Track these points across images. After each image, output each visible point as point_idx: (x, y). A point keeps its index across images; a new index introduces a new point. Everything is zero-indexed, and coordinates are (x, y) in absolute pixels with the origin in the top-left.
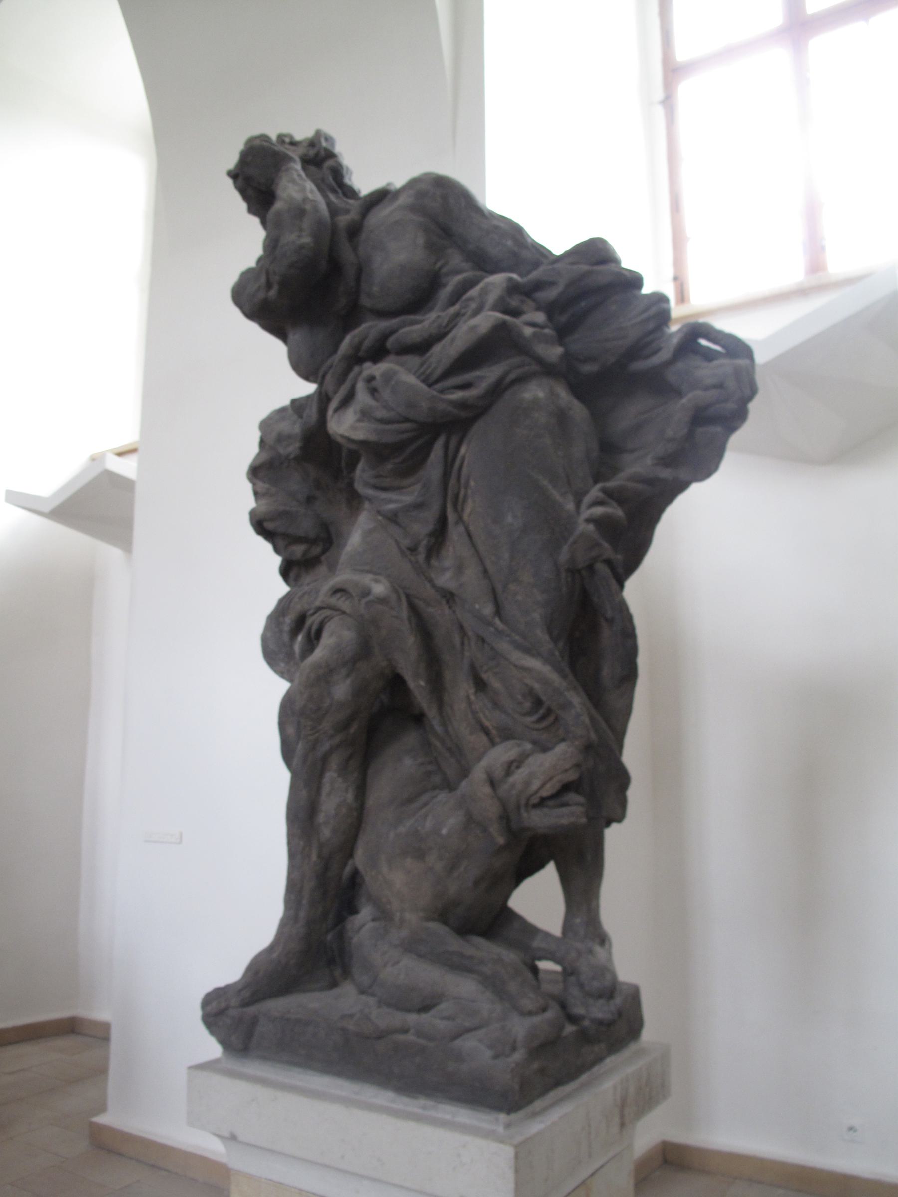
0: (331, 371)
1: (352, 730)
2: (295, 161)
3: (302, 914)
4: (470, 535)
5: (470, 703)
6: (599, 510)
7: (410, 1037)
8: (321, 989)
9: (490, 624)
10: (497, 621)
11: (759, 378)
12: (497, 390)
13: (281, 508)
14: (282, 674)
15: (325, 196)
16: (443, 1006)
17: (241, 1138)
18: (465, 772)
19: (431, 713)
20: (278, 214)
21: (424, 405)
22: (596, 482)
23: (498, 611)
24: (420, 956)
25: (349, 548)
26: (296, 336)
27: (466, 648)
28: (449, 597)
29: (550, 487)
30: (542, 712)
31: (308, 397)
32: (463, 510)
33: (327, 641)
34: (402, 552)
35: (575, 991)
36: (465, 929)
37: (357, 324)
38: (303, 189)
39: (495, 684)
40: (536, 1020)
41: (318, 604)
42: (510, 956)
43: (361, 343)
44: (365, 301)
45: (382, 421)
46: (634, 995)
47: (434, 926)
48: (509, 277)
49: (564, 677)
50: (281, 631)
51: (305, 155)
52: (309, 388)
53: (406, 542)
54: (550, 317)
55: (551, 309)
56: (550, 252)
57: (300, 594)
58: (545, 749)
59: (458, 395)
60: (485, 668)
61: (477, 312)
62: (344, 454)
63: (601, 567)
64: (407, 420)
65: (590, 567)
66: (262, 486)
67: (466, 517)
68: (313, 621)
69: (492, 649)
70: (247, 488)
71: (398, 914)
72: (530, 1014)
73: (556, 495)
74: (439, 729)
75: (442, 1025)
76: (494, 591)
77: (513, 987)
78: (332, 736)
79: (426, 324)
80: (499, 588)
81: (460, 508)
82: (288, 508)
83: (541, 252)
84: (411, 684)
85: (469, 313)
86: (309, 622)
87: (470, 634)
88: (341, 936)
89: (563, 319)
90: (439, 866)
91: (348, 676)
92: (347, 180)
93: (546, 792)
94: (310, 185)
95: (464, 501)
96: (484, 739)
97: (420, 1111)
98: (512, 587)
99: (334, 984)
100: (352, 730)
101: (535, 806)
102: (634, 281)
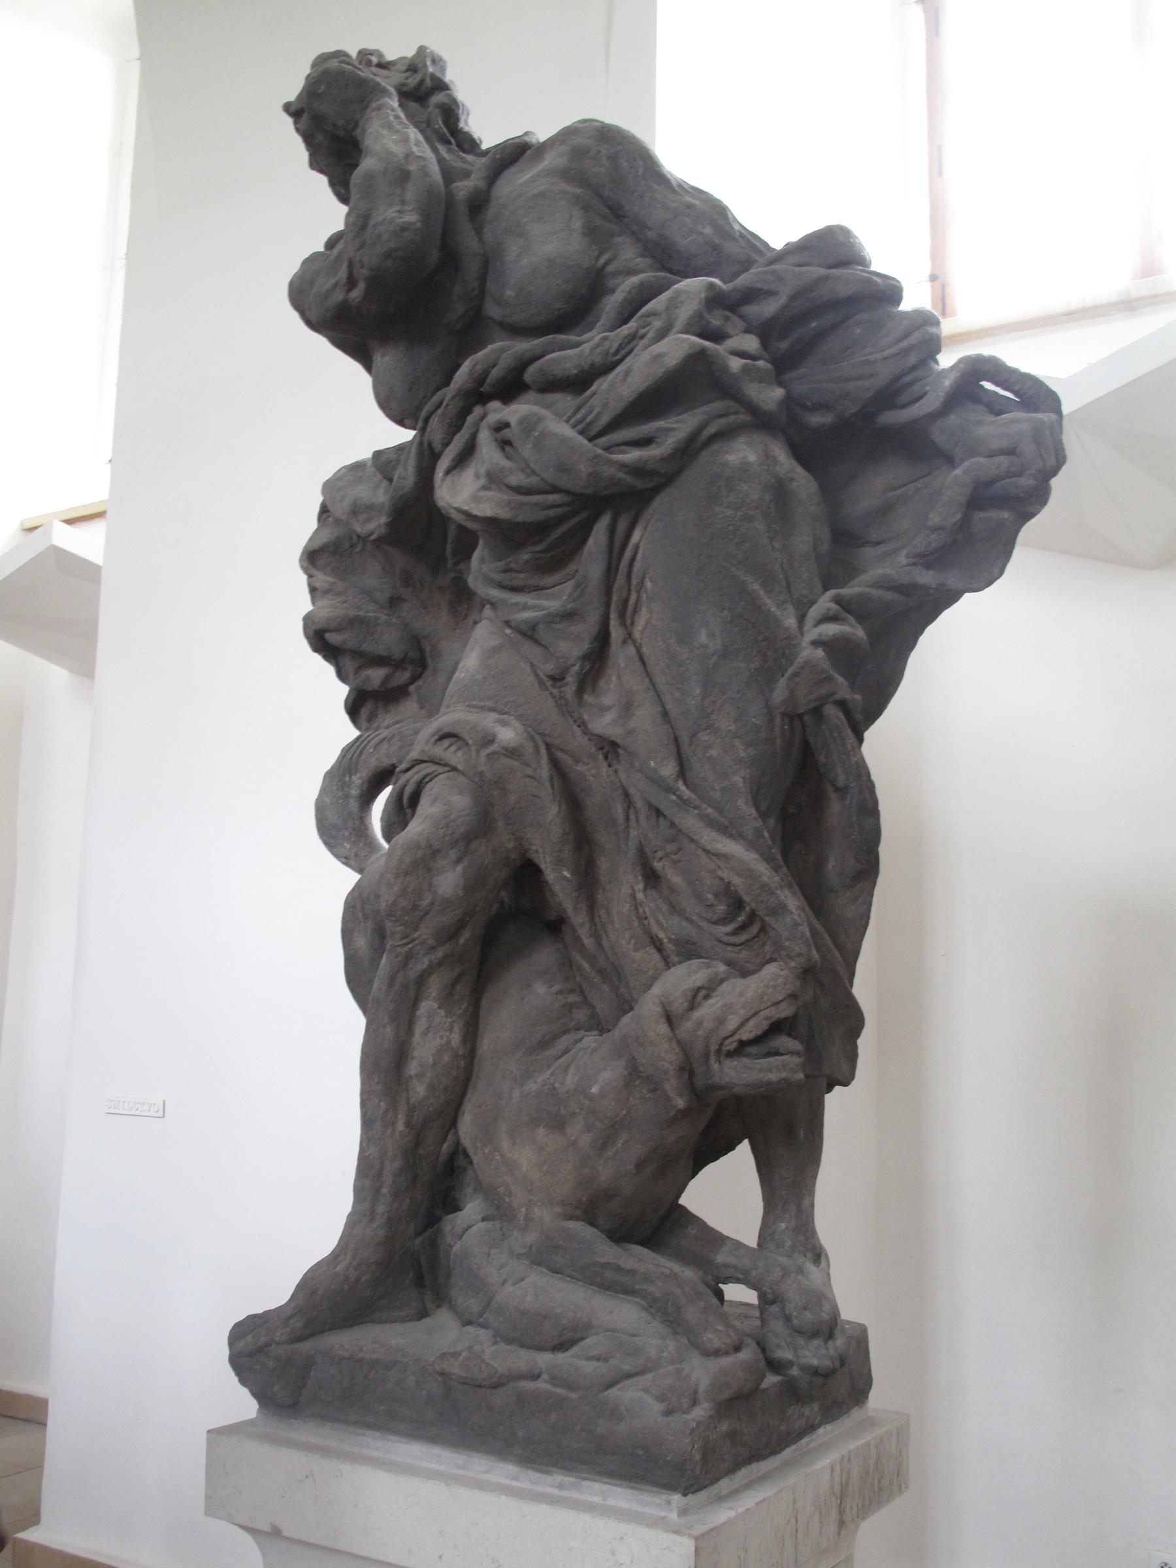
0: (440, 411)
1: (462, 941)
2: (390, 96)
3: (381, 1208)
5: (636, 906)
6: (831, 629)
7: (542, 1385)
8: (404, 1320)
9: (672, 790)
10: (681, 785)
11: (1071, 440)
12: (689, 450)
13: (352, 613)
14: (346, 860)
15: (435, 150)
16: (589, 1341)
17: (285, 1534)
18: (626, 1005)
19: (578, 919)
20: (370, 176)
21: (584, 469)
22: (826, 589)
23: (683, 772)
24: (554, 1271)
25: (459, 675)
26: (385, 359)
27: (633, 823)
28: (610, 748)
29: (762, 592)
30: (741, 918)
31: (400, 448)
32: (632, 623)
33: (427, 809)
34: (541, 682)
35: (778, 1326)
36: (621, 1235)
37: (481, 345)
38: (405, 140)
39: (675, 878)
40: (727, 1361)
41: (414, 754)
42: (689, 1273)
43: (486, 373)
44: (493, 311)
45: (518, 490)
46: (860, 1340)
48: (709, 282)
49: (776, 869)
50: (347, 796)
51: (403, 85)
53: (549, 667)
54: (765, 344)
55: (766, 331)
56: (766, 244)
58: (745, 974)
59: (633, 455)
60: (660, 854)
61: (662, 335)
62: (452, 532)
63: (831, 710)
64: (555, 490)
65: (817, 711)
66: (323, 579)
67: (637, 634)
69: (672, 825)
70: (301, 581)
71: (523, 1210)
72: (718, 1353)
73: (770, 604)
74: (588, 942)
75: (589, 1367)
76: (676, 740)
77: (692, 1314)
78: (432, 949)
79: (586, 347)
80: (685, 739)
81: (628, 621)
82: (361, 614)
83: (753, 244)
84: (550, 875)
85: (651, 335)
87: (639, 804)
88: (434, 1244)
89: (783, 345)
90: (585, 1140)
91: (458, 861)
94: (414, 133)
95: (635, 611)
96: (656, 957)
97: (555, 1491)
98: (704, 737)
99: (423, 1314)
100: (462, 941)
101: (730, 1054)
102: (890, 292)
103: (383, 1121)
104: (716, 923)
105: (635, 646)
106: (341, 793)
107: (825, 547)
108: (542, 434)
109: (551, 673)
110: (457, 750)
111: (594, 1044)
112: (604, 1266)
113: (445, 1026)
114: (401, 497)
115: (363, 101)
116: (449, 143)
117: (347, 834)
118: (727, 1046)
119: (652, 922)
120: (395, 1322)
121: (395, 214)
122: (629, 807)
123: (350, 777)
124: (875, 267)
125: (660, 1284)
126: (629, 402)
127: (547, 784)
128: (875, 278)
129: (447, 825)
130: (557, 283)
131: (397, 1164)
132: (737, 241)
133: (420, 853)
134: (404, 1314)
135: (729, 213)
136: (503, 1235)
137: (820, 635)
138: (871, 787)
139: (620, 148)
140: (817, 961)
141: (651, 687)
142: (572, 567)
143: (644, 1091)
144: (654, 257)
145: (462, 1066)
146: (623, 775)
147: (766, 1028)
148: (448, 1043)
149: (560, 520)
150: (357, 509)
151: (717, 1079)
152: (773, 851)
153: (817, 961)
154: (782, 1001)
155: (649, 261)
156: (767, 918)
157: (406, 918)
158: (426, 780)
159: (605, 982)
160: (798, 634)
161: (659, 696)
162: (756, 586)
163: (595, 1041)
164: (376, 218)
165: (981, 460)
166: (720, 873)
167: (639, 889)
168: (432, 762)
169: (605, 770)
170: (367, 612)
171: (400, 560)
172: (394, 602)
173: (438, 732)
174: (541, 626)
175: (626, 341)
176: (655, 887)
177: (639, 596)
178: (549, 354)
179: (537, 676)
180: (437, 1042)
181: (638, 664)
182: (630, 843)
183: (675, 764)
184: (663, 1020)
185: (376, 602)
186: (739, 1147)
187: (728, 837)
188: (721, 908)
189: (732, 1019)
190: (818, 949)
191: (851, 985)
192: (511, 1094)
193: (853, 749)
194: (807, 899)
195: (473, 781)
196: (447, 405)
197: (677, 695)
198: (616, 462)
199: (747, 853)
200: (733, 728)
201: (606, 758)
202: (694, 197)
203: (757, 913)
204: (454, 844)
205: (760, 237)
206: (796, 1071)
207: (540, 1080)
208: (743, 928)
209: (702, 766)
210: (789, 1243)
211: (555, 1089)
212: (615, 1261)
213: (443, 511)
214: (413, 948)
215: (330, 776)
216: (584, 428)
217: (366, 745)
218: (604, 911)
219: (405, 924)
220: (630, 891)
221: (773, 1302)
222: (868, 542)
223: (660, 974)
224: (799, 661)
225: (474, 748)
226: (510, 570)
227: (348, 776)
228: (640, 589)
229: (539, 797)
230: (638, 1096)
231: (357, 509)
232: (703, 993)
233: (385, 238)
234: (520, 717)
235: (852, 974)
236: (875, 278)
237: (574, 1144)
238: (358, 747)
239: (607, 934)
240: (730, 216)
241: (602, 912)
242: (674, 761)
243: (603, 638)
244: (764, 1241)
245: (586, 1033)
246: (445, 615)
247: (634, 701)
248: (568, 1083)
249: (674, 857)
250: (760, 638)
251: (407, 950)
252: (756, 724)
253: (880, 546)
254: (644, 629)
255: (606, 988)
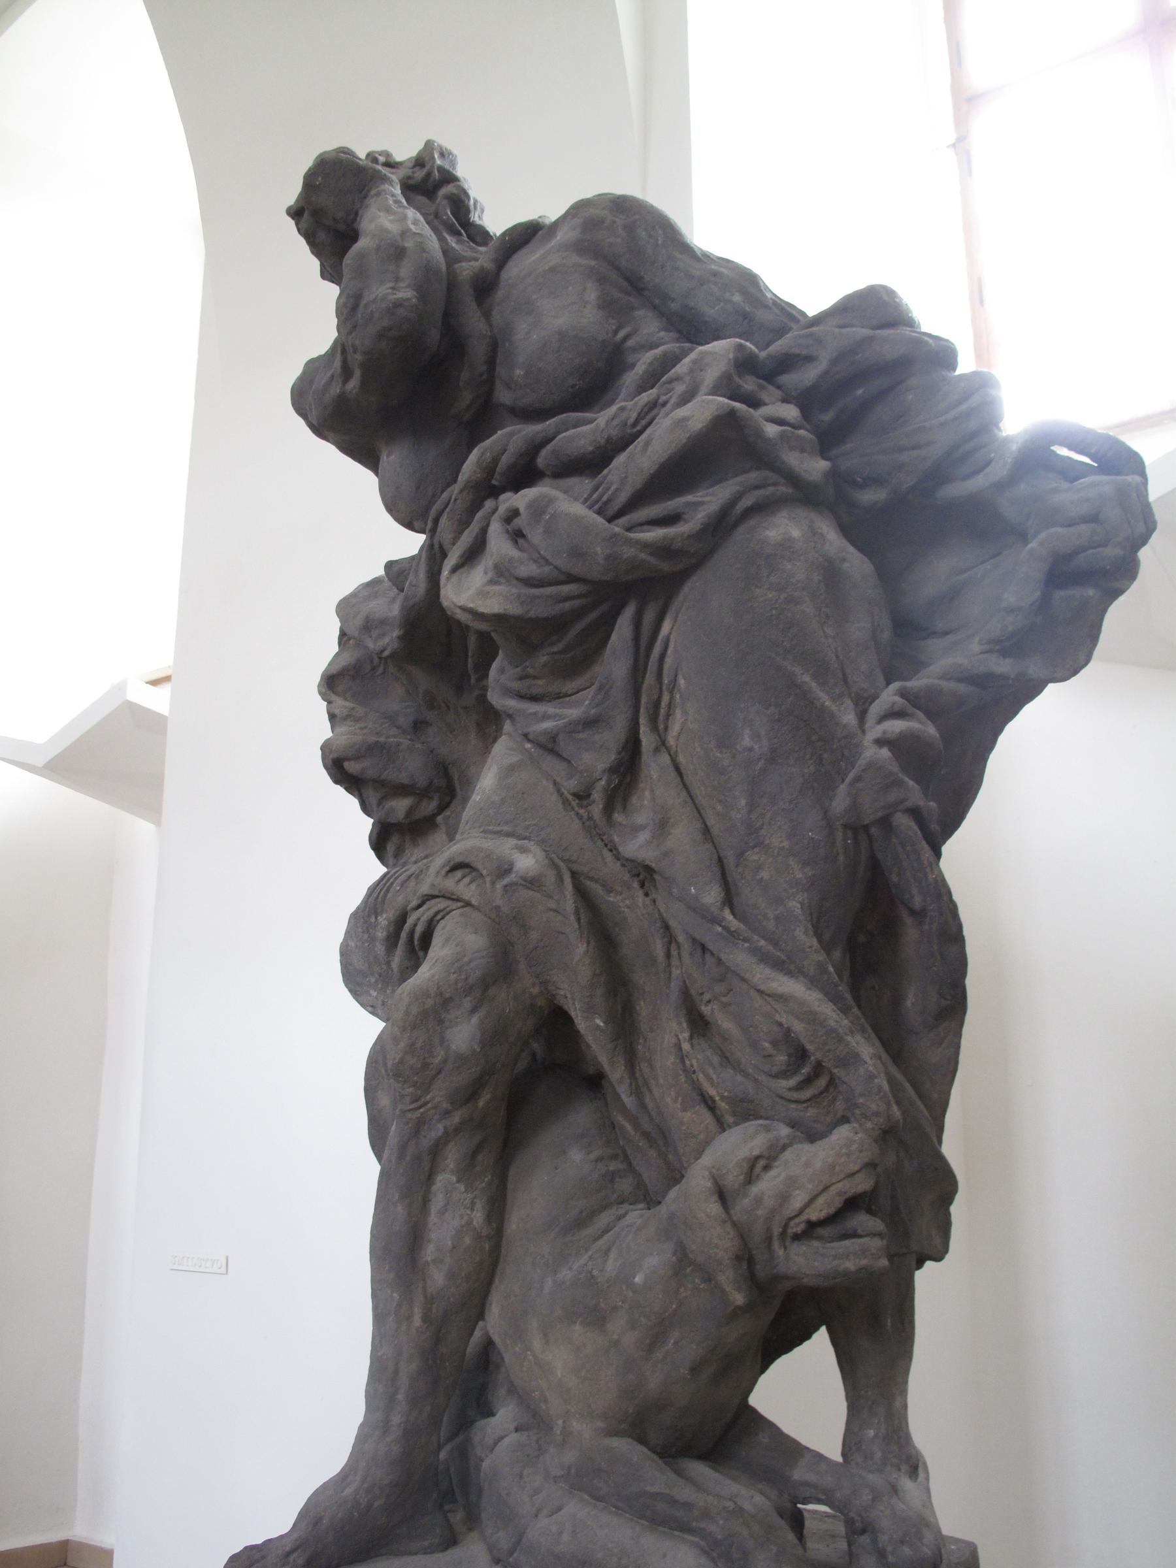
1: (481, 1104)
3: (396, 1419)
4: (677, 769)
6: (896, 726)
8: (427, 1551)
9: (715, 920)
10: (727, 914)
13: (372, 739)
14: (373, 1010)
15: (442, 240)
18: (675, 1176)
19: (616, 1074)
20: (362, 255)
21: (600, 550)
23: (729, 899)
25: (476, 797)
26: (391, 457)
27: (675, 961)
29: (814, 685)
30: (805, 1070)
32: (666, 729)
33: (440, 950)
34: (565, 802)
38: (404, 218)
39: (724, 1022)
41: (425, 889)
43: (496, 461)
44: (503, 396)
45: (529, 582)
47: (623, 1445)
49: (845, 1010)
50: (372, 939)
51: (409, 178)
52: (410, 543)
53: (571, 785)
55: (806, 401)
57: (402, 878)
58: (813, 1137)
60: (707, 997)
63: (903, 821)
64: (571, 579)
65: (885, 822)
66: (341, 704)
67: (671, 741)
68: (418, 919)
69: (720, 962)
71: (560, 1422)
74: (628, 1101)
76: (720, 860)
78: (447, 1113)
80: (730, 859)
81: (661, 726)
82: (382, 739)
83: (787, 314)
84: (581, 1025)
86: (410, 921)
87: (681, 938)
88: (463, 1454)
89: (828, 417)
90: (630, 1339)
91: (473, 1011)
92: (475, 217)
93: (815, 1213)
96: (708, 1118)
98: (753, 856)
99: (451, 1541)
100: (481, 1104)
101: (797, 1237)
103: (396, 1316)
104: (776, 1076)
105: (670, 755)
106: (366, 936)
107: (886, 635)
108: (552, 516)
109: (576, 790)
110: (471, 882)
111: (640, 1220)
112: (655, 1496)
113: (465, 1203)
114: (413, 606)
115: (363, 190)
116: (459, 234)
117: (373, 980)
118: (792, 1228)
119: (701, 1077)
120: (416, 1553)
121: (388, 291)
122: (670, 942)
123: (376, 918)
124: (925, 328)
125: (721, 1522)
126: (650, 474)
127: (572, 918)
128: (928, 339)
129: (460, 970)
130: (570, 356)
131: (414, 1366)
132: (770, 309)
133: (430, 1003)
134: (426, 1543)
135: (761, 281)
136: (540, 1448)
137: (884, 732)
138: (953, 909)
139: (637, 217)
140: (899, 1120)
141: (689, 800)
142: (597, 668)
143: (697, 1280)
144: (679, 331)
145: (487, 1249)
146: (661, 906)
147: (840, 1206)
148: (470, 1223)
149: (579, 614)
150: (369, 624)
151: (782, 1269)
152: (840, 988)
153: (899, 1120)
154: (858, 1172)
155: (674, 335)
156: (835, 1071)
157: (415, 1078)
158: (439, 917)
159: (651, 1147)
160: (859, 732)
161: (699, 812)
162: (807, 678)
163: (642, 1216)
164: (368, 297)
165: (1059, 530)
166: (778, 1018)
167: (685, 1039)
168: (443, 896)
169: (640, 900)
170: (388, 737)
171: (424, 680)
172: (419, 726)
173: (449, 861)
174: (561, 737)
175: (646, 409)
176: (704, 1035)
177: (672, 697)
178: (563, 432)
179: (562, 795)
180: (457, 1222)
181: (674, 774)
182: (673, 984)
183: (720, 889)
184: (715, 1198)
185: (398, 727)
186: (816, 1336)
187: (785, 974)
188: (782, 1058)
189: (798, 1195)
190: (898, 1103)
191: (940, 1142)
192: (542, 1283)
193: (931, 865)
194: (884, 1043)
195: (490, 918)
196: (456, 500)
197: (719, 808)
198: (637, 542)
199: (808, 992)
200: (786, 844)
201: (642, 886)
202: (721, 266)
203: (824, 1064)
204: (468, 991)
205: (795, 307)
206: (879, 1258)
207: (575, 1267)
208: (808, 1081)
209: (752, 891)
210: (879, 1454)
211: (593, 1277)
212: (667, 1491)
213: (449, 613)
214: (425, 1112)
215: (355, 917)
216: (600, 508)
217: (392, 884)
218: (646, 1064)
219: (414, 1085)
220: (674, 1040)
221: (863, 1531)
222: (934, 633)
223: (713, 1138)
224: (861, 763)
225: (488, 879)
226: (527, 677)
227: (373, 917)
228: (674, 687)
229: (564, 933)
230: (690, 1286)
231: (369, 624)
232: (762, 1163)
233: (376, 315)
234: (542, 842)
235: (941, 1129)
236: (928, 339)
237: (616, 1344)
238: (385, 884)
239: (650, 1091)
240: (762, 284)
241: (644, 1066)
242: (718, 886)
243: (632, 748)
244: (849, 1451)
245: (632, 1206)
246: (473, 739)
247: (669, 818)
248: (609, 1269)
249: (724, 999)
250: (814, 738)
251: (419, 1115)
252: (813, 839)
253: (949, 636)
254: (679, 734)
255: (653, 1153)
